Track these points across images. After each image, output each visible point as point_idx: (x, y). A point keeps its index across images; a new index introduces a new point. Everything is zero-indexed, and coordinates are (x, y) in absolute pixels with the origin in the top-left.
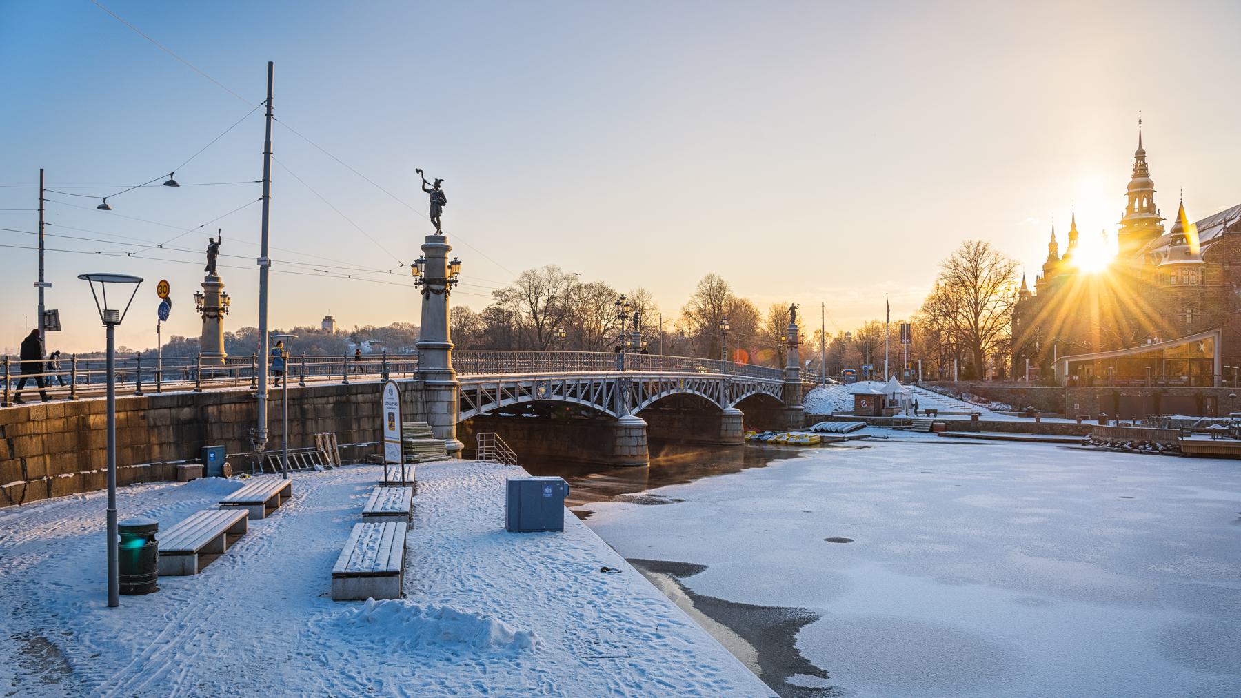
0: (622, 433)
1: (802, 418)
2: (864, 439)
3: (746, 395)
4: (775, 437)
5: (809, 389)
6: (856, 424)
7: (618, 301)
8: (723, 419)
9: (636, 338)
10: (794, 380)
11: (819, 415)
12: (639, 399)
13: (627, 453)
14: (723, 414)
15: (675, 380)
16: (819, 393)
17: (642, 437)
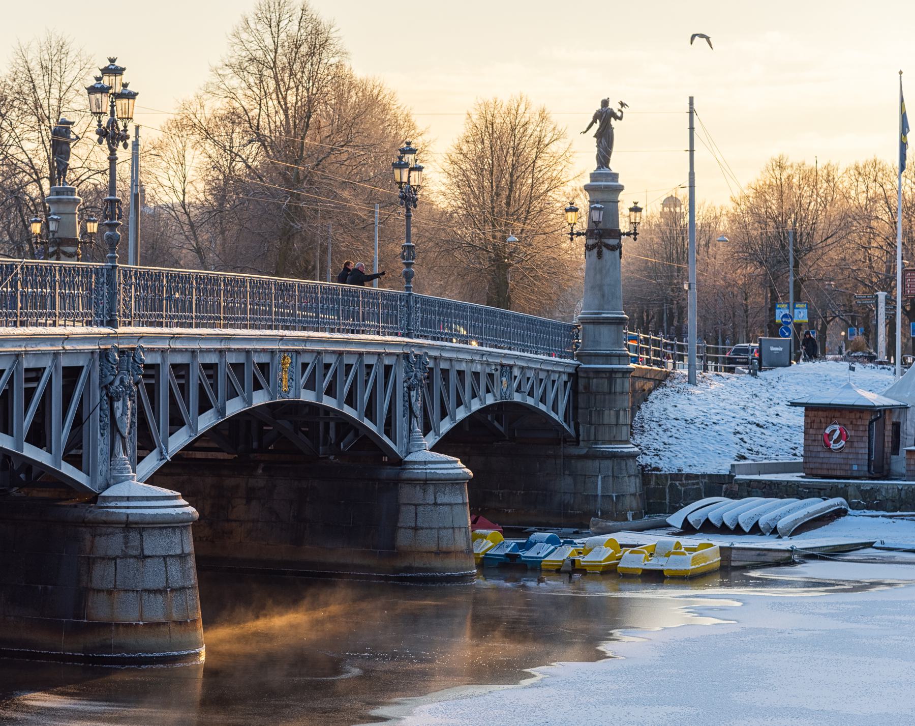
0: (113, 544)
1: (632, 485)
2: (852, 556)
3: (468, 407)
4: (567, 552)
5: (650, 384)
6: (816, 506)
7: (98, 79)
8: (406, 494)
9: (62, 208)
10: (608, 357)
11: (689, 476)
12: (159, 424)
13: (132, 616)
14: (406, 475)
15: (265, 359)
16: (681, 401)
17: (182, 557)
